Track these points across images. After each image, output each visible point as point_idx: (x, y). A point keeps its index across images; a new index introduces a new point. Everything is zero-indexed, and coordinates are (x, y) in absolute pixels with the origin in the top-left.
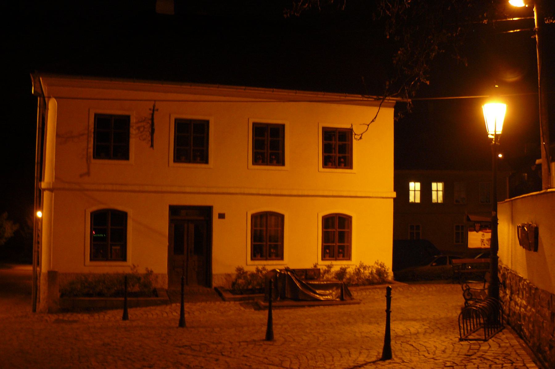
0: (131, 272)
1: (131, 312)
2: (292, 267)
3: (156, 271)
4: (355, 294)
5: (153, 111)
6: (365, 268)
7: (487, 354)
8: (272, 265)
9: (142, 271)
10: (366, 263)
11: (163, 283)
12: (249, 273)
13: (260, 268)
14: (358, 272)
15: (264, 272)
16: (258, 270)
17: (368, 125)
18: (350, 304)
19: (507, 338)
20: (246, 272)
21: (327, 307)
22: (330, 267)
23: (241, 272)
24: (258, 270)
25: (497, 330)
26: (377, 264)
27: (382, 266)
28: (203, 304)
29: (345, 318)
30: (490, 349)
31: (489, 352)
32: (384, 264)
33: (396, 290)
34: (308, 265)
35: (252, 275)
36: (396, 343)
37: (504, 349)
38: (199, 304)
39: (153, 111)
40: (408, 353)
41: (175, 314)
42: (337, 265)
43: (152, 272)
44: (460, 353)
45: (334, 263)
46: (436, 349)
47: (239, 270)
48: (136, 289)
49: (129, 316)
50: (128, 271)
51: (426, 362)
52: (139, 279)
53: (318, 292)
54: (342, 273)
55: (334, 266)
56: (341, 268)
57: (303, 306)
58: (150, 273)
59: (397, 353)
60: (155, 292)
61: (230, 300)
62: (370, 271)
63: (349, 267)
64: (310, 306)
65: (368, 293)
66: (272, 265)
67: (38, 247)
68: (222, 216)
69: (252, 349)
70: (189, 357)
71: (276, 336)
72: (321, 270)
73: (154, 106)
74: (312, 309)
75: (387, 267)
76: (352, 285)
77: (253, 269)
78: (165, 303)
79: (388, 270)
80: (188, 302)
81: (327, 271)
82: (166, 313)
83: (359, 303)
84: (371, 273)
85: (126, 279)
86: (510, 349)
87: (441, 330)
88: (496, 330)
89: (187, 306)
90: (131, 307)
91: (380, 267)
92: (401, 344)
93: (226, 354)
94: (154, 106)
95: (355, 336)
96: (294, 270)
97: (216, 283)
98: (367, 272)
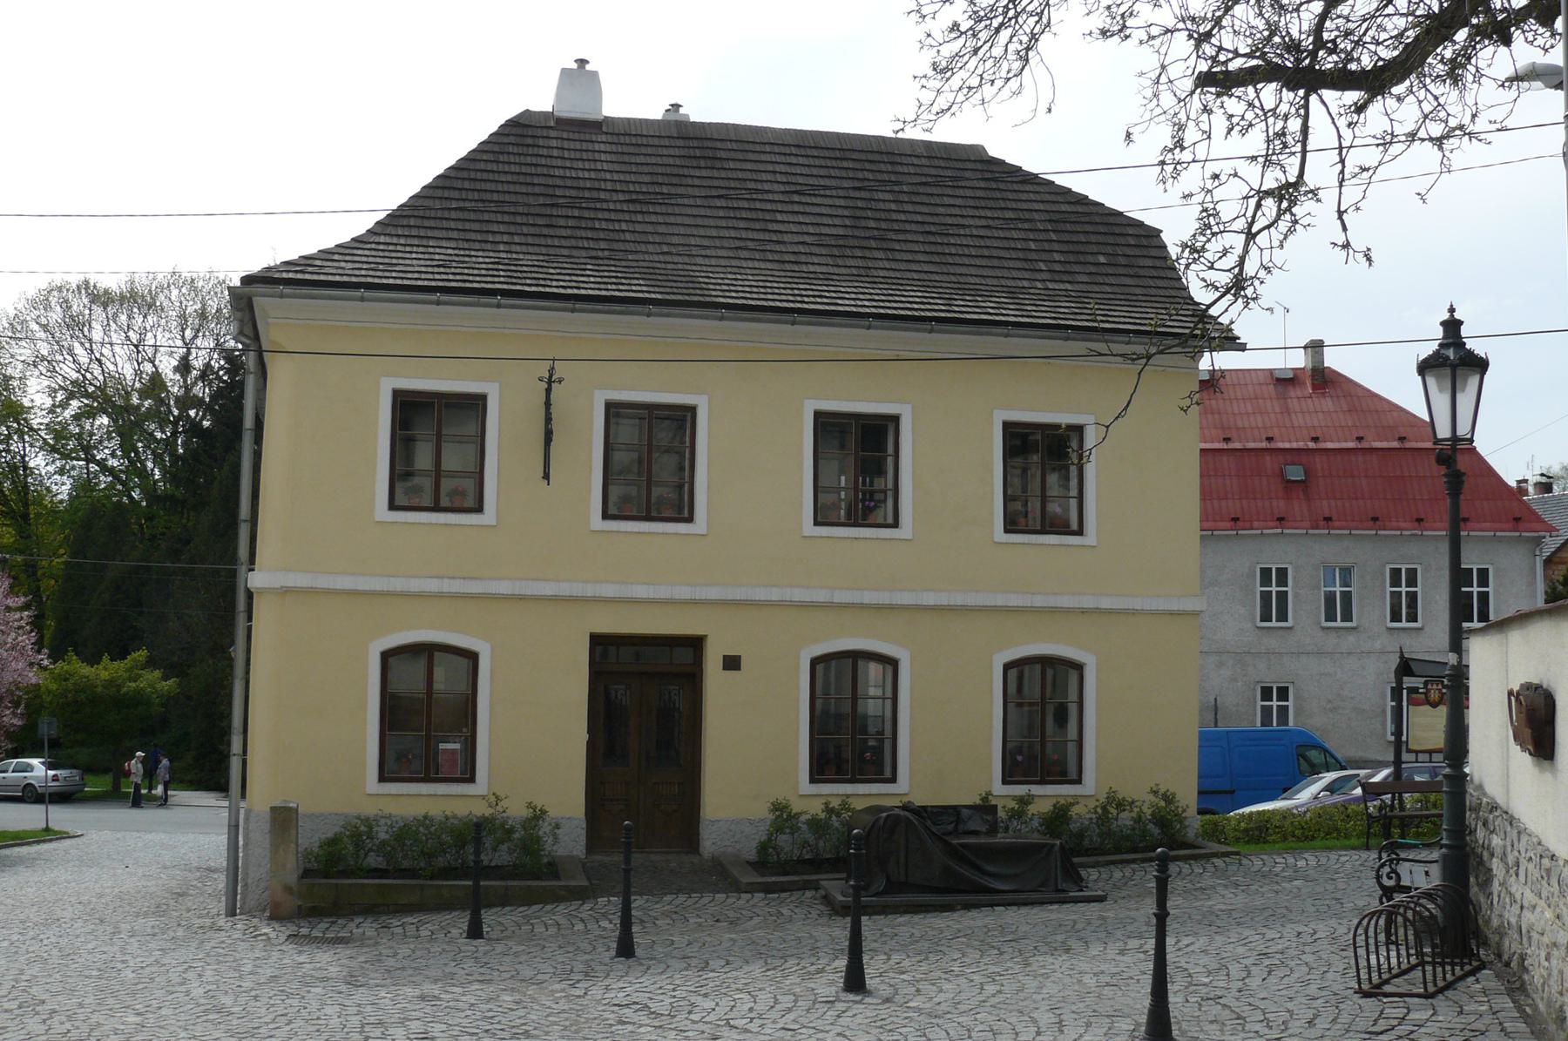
0: (488, 812)
1: (489, 917)
2: (919, 800)
3: (553, 812)
4: (1091, 875)
5: (550, 382)
6: (1121, 805)
7: (1423, 1030)
8: (863, 794)
9: (516, 810)
10: (1126, 791)
11: (571, 841)
12: (804, 818)
13: (835, 803)
14: (1103, 817)
15: (846, 815)
16: (829, 810)
17: (1107, 427)
18: (1076, 901)
19: (1484, 992)
20: (798, 815)
21: (1015, 908)
22: (1024, 801)
23: (783, 816)
24: (829, 810)
25: (1462, 969)
26: (1155, 793)
27: (1169, 798)
28: (682, 898)
29: (1060, 938)
30: (1433, 1018)
31: (1429, 1024)
32: (1174, 795)
33: (1208, 866)
34: (964, 795)
35: (814, 824)
36: (1187, 1001)
37: (1473, 1018)
38: (668, 898)
39: (550, 382)
40: (1214, 1026)
41: (604, 923)
42: (1046, 796)
43: (543, 812)
44: (1353, 1028)
45: (1036, 790)
46: (1291, 1016)
47: (779, 808)
48: (503, 857)
49: (486, 929)
50: (481, 810)
51: (944, 834)
52: (511, 831)
53: (989, 868)
54: (1059, 817)
55: (1036, 800)
56: (1054, 805)
57: (949, 908)
58: (538, 816)
59: (1184, 1026)
60: (553, 869)
61: (751, 889)
62: (1134, 815)
63: (1078, 803)
64: (968, 907)
65: (1128, 874)
66: (863, 794)
67: (182, 782)
68: (732, 663)
69: (808, 1011)
70: (642, 1030)
71: (870, 983)
72: (999, 808)
73: (551, 371)
74: (974, 913)
75: (1182, 804)
76: (1087, 852)
77: (816, 809)
78: (581, 895)
79: (1184, 811)
80: (641, 894)
81: (1018, 814)
82: (582, 920)
83: (1101, 899)
84: (1138, 820)
85: (478, 830)
86: (1488, 1019)
87: (1212, 913)
88: (1457, 968)
89: (638, 902)
90: (490, 906)
91: (1163, 804)
92: (1200, 1005)
93: (740, 1023)
94: (551, 371)
95: (1080, 981)
96: (924, 808)
97: (711, 841)
98: (1126, 818)
